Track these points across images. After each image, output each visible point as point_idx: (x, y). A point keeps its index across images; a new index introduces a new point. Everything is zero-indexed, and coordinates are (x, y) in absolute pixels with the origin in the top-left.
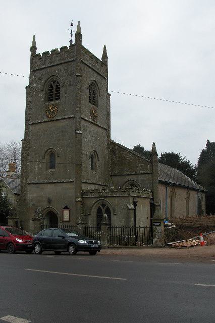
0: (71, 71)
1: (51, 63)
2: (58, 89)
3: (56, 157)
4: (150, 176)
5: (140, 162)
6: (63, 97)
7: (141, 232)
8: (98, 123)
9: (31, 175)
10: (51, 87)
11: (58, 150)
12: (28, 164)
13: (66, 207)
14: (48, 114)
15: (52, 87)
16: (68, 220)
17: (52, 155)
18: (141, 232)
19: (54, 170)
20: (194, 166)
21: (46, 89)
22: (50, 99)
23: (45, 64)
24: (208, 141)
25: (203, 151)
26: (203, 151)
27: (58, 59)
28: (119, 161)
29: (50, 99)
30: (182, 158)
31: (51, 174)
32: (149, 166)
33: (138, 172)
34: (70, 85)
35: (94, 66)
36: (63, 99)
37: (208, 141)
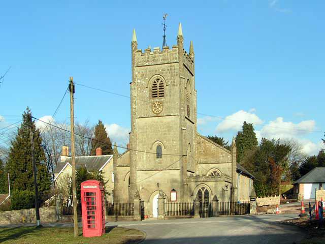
2: (161, 86)
4: (230, 164)
5: (222, 153)
8: (190, 119)
13: (174, 190)
14: (154, 110)
16: (175, 200)
19: (161, 159)
20: (46, 132)
21: (151, 85)
22: (154, 95)
23: (148, 61)
24: (245, 122)
25: (239, 133)
26: (239, 134)
27: (161, 58)
28: (204, 151)
29: (154, 95)
30: (225, 142)
31: (159, 163)
34: (174, 85)
35: (188, 65)
37: (245, 122)
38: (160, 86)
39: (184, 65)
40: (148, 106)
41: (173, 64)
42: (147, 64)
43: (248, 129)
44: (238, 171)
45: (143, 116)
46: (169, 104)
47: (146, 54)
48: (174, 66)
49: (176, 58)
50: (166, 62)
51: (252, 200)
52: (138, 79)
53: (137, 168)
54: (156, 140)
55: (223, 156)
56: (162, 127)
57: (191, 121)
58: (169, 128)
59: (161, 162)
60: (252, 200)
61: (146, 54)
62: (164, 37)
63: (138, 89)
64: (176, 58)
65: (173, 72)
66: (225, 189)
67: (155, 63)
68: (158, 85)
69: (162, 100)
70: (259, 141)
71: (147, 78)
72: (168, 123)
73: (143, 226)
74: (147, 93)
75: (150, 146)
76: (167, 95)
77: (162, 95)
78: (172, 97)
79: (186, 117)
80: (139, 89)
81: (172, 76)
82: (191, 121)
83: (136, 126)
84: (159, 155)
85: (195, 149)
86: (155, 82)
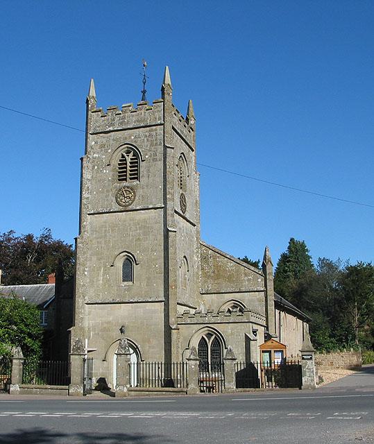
0: (156, 140)
1: (121, 123)
2: (135, 164)
3: (272, 269)
6: (143, 176)
7: (148, 377)
8: (187, 216)
9: (92, 290)
10: (123, 160)
11: (138, 255)
12: (86, 273)
15: (125, 160)
17: (129, 262)
18: (148, 377)
19: (131, 283)
21: (116, 162)
22: (122, 177)
23: (112, 125)
24: (292, 240)
27: (134, 119)
28: (214, 272)
32: (260, 280)
33: (243, 289)
36: (143, 180)
37: (292, 240)
38: (131, 167)
39: (173, 128)
40: (111, 193)
41: (154, 127)
42: (111, 129)
43: (296, 252)
44: (278, 306)
45: (100, 210)
46: (145, 190)
47: (110, 114)
48: (156, 130)
49: (160, 119)
50: (142, 125)
51: (305, 357)
52: (94, 153)
53: (86, 298)
54: (121, 250)
55: (249, 280)
56: (134, 228)
57: (188, 221)
58: (145, 228)
59: (129, 288)
60: (305, 357)
61: (110, 114)
62: (144, 92)
63: (94, 167)
64: (160, 119)
65: (154, 139)
66: (251, 336)
67: (124, 127)
68: (129, 161)
69: (135, 183)
70: (315, 261)
71: (109, 151)
72: (145, 221)
73: (169, 387)
74: (109, 173)
75: (111, 260)
76: (143, 176)
77: (136, 176)
78: (151, 179)
79: (176, 212)
80: (96, 167)
81: (152, 145)
82: (188, 221)
83: (88, 228)
84: (128, 276)
85: (198, 267)
86: (123, 156)
